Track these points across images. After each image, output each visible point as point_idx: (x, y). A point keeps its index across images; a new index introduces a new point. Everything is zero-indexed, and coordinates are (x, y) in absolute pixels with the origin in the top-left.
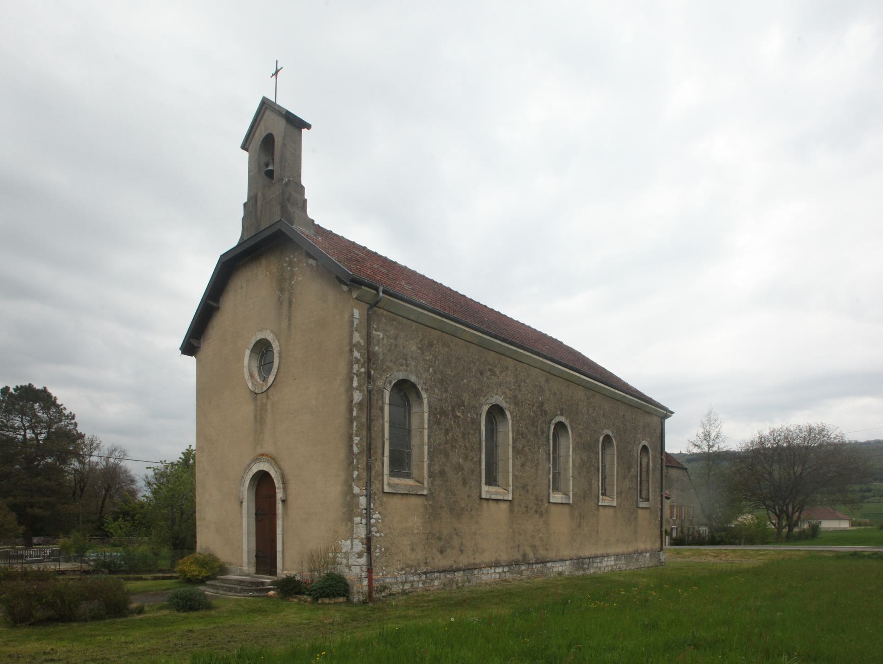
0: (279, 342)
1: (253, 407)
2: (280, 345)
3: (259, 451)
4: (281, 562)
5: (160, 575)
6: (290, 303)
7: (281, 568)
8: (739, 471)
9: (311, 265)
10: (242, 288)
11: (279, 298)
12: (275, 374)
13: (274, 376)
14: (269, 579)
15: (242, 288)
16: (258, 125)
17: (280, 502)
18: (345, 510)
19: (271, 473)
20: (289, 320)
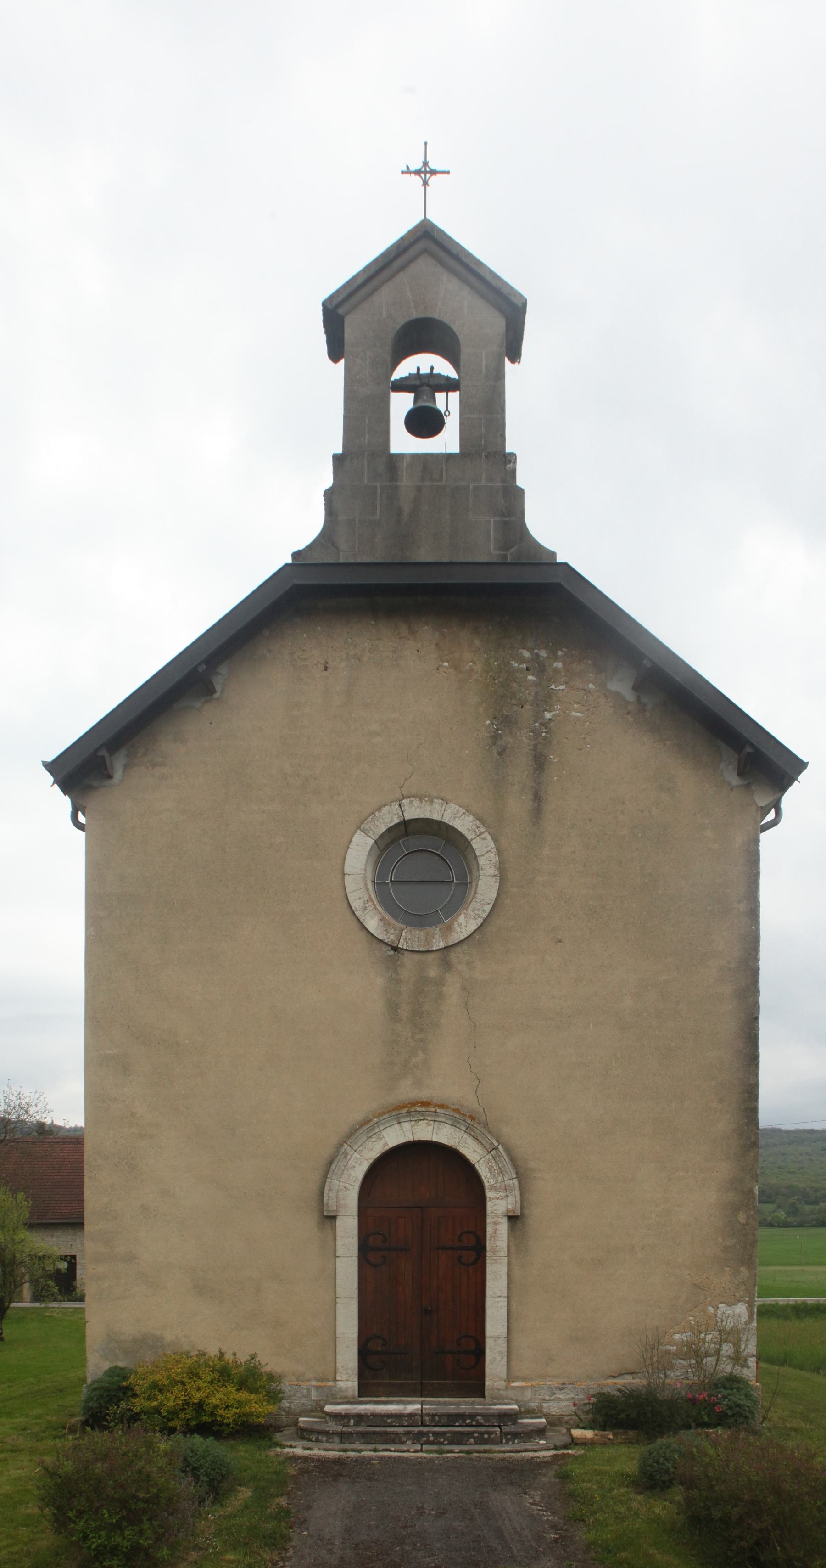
0: (495, 840)
1: (380, 982)
2: (499, 851)
3: (407, 1091)
4: (502, 1346)
5: (534, 1415)
6: (540, 762)
7: (502, 1371)
8: (100, 1482)
9: (618, 694)
10: (326, 669)
11: (495, 738)
12: (484, 915)
13: (480, 921)
14: (477, 1409)
15: (326, 669)
16: (403, 268)
17: (503, 1227)
18: (730, 1242)
19: (464, 1151)
20: (537, 797)
